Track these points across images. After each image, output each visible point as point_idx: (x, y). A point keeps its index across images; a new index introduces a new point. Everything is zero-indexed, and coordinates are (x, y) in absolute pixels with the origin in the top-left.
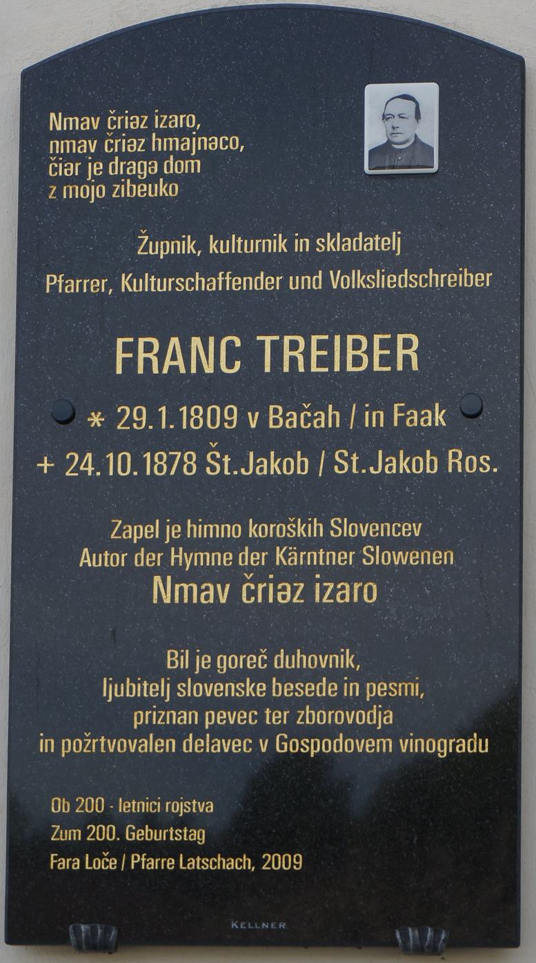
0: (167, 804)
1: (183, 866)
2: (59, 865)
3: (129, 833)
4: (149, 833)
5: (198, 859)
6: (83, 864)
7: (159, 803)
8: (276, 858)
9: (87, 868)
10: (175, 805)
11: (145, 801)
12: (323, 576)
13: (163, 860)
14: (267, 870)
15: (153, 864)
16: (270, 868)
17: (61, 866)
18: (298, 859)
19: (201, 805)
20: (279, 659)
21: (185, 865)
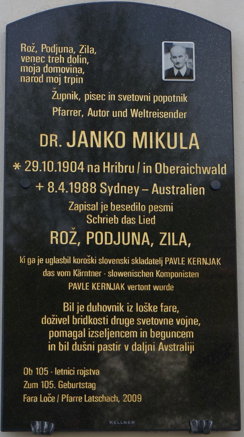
0: (78, 371)
1: (86, 400)
2: (27, 400)
3: (60, 385)
4: (69, 384)
5: (93, 397)
6: (39, 399)
7: (74, 370)
8: (130, 396)
9: (41, 401)
10: (82, 371)
11: (67, 369)
12: (24, 73)
13: (77, 397)
14: (125, 402)
15: (72, 399)
16: (126, 401)
17: (29, 400)
18: (139, 397)
19: (94, 371)
20: (113, 320)
21: (87, 399)
